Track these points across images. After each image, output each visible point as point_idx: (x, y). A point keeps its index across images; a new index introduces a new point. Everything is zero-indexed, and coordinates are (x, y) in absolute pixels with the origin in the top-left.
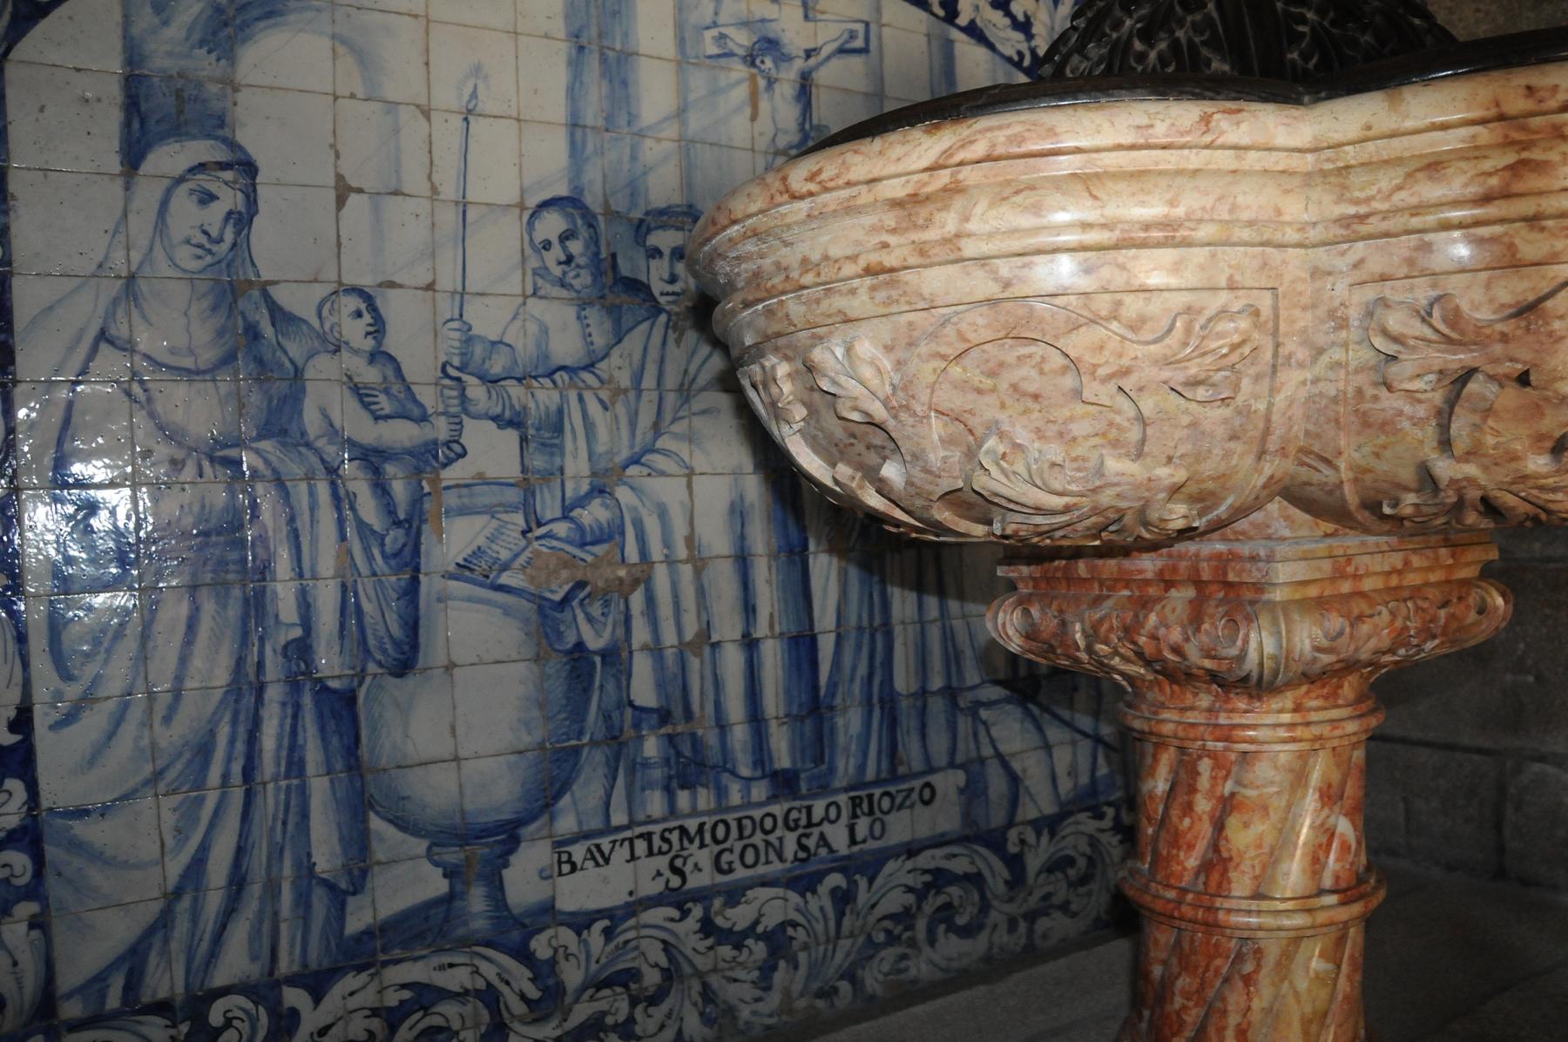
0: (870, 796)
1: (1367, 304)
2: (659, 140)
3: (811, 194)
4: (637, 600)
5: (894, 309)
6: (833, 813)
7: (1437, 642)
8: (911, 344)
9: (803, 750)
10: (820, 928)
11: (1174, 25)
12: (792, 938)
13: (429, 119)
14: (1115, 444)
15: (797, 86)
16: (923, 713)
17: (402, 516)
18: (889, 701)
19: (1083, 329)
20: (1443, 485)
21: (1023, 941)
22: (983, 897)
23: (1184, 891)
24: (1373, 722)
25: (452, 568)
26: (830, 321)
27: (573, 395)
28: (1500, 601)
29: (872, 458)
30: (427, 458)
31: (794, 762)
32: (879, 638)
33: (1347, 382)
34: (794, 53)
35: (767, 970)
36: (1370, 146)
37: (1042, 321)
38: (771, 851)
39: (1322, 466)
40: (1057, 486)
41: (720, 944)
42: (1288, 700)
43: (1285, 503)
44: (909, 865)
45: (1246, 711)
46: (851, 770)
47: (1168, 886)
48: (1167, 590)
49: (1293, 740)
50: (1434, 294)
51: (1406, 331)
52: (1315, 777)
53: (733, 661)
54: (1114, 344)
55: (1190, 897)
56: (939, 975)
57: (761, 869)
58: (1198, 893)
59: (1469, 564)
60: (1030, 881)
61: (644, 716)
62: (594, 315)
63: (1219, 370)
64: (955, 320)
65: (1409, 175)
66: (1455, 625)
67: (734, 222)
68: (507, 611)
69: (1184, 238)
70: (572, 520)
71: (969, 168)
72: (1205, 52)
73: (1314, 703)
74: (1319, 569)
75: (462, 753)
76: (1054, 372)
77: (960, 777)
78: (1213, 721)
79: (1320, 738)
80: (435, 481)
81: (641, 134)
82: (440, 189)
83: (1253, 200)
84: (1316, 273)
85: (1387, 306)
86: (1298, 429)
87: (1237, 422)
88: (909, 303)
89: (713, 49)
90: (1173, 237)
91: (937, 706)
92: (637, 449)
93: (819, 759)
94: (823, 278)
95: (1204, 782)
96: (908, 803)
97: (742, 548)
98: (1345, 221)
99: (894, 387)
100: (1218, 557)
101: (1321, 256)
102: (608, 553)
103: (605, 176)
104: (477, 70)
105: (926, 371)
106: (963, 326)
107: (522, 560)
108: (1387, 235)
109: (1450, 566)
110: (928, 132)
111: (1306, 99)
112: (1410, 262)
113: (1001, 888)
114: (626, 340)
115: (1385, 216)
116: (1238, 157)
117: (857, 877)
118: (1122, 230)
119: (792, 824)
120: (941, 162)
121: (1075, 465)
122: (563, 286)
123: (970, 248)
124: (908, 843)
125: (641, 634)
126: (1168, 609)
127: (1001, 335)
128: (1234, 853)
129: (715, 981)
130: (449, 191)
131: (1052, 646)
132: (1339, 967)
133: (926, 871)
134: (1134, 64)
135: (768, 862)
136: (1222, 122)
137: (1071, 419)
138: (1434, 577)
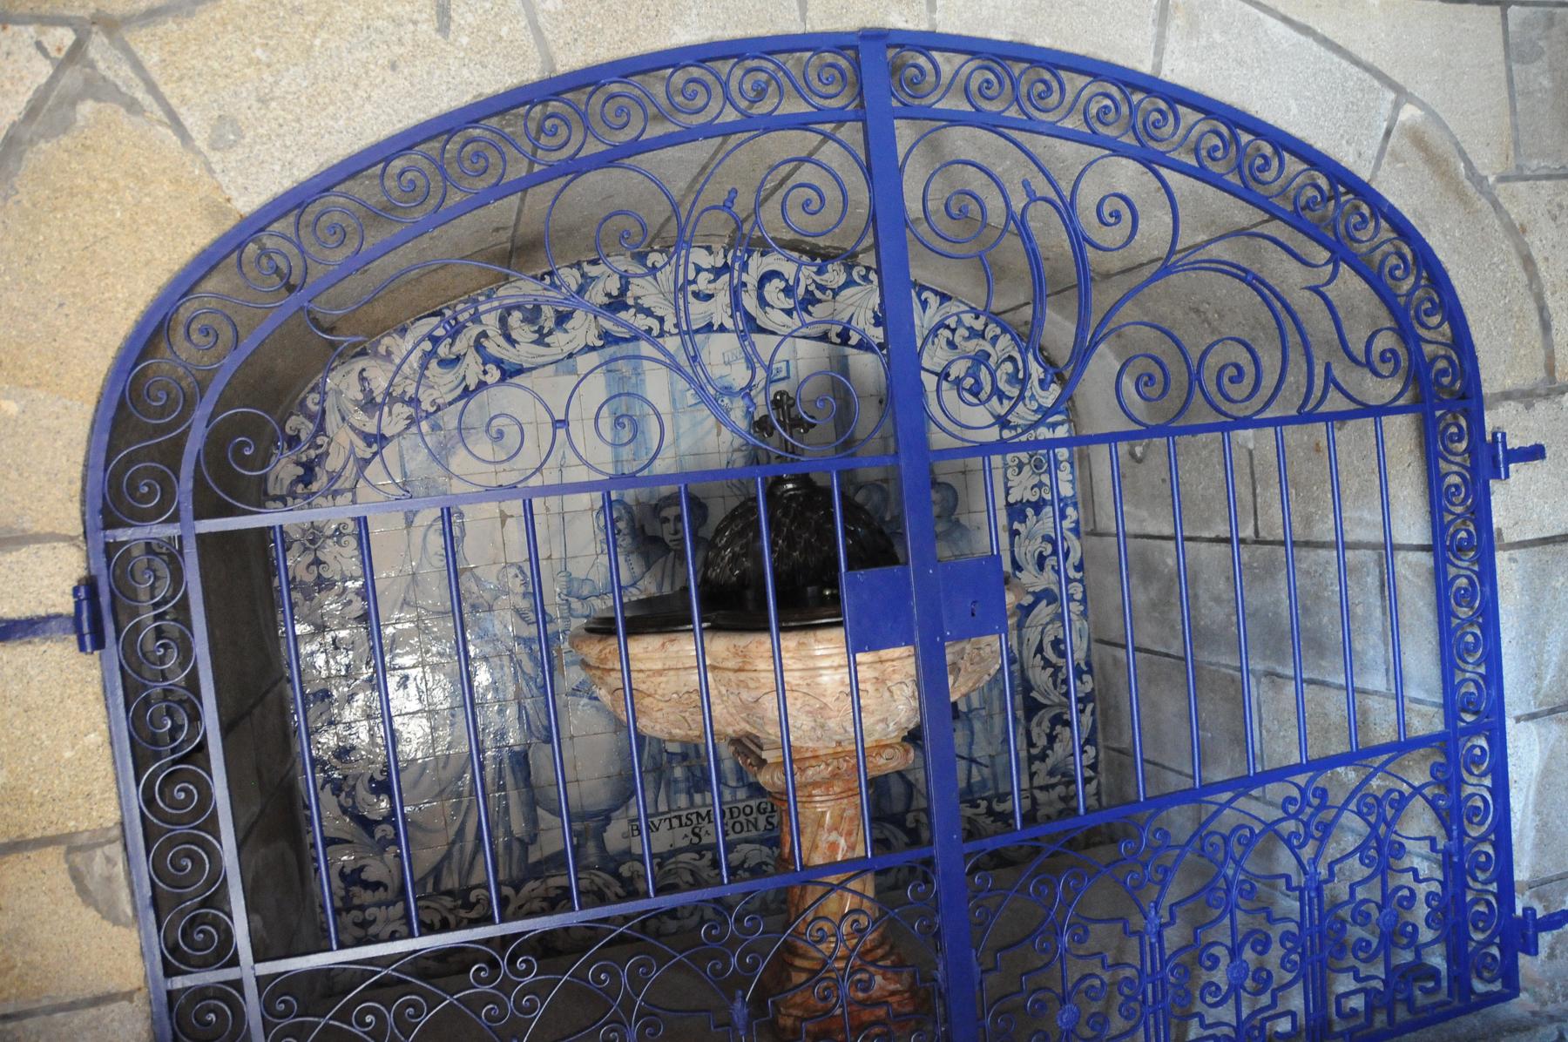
57: (744, 835)
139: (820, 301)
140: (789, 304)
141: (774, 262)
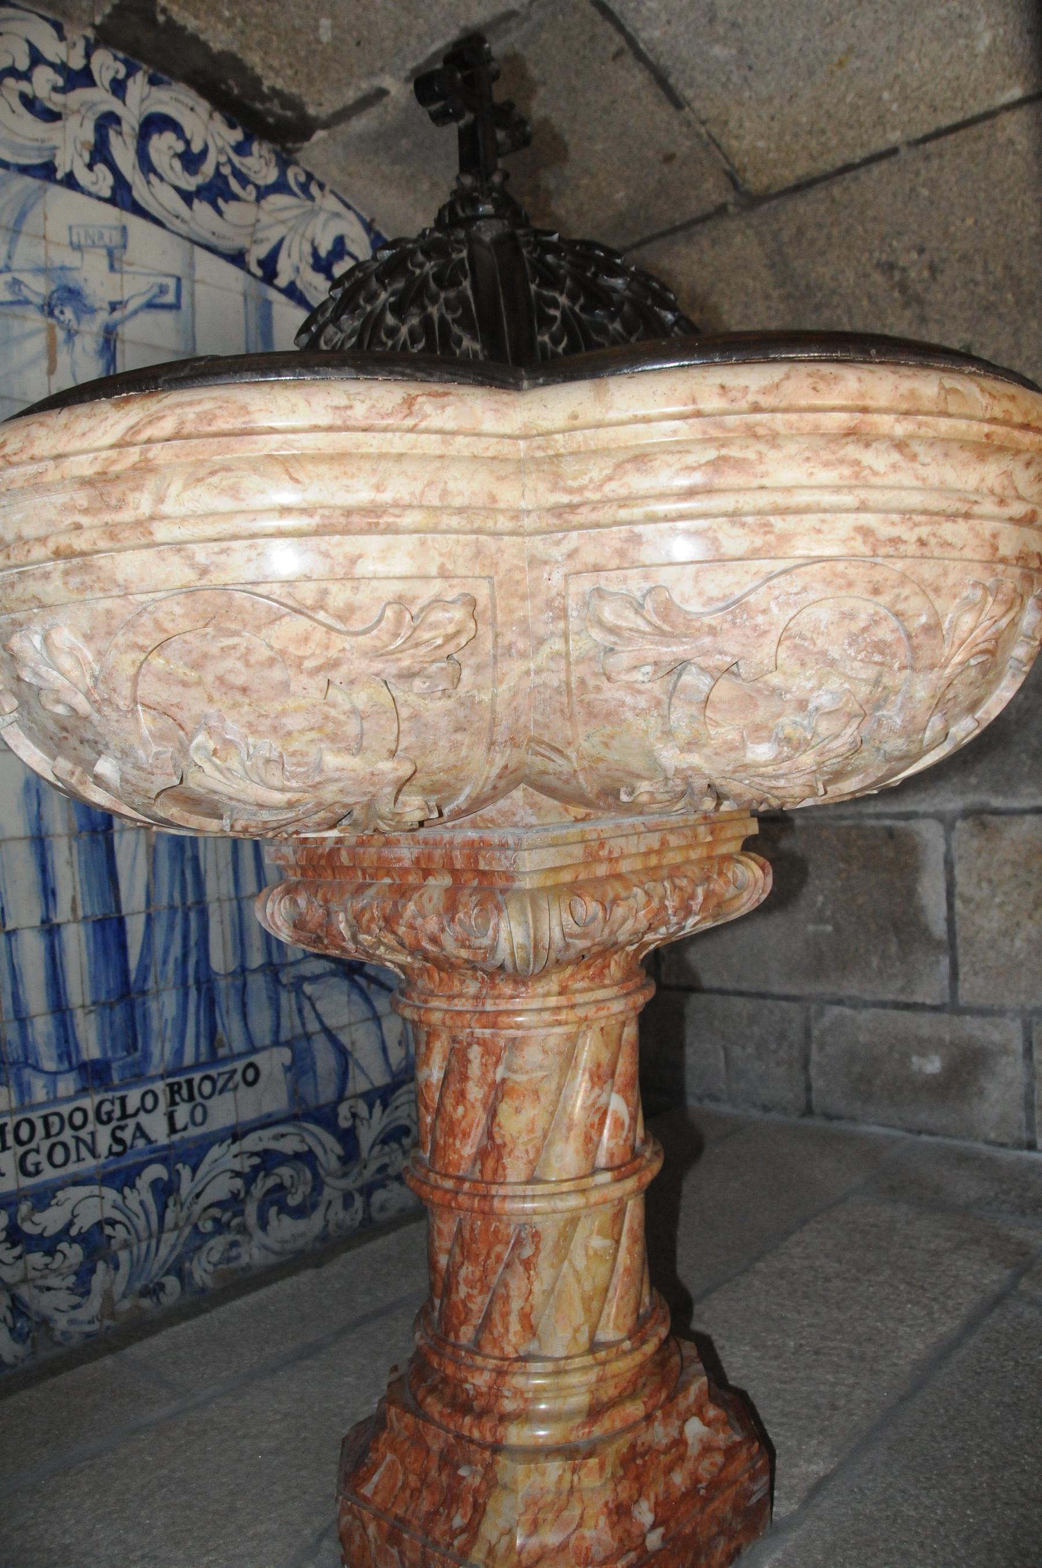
0: (190, 1082)
5: (88, 595)
6: (149, 1102)
9: (113, 1039)
10: (141, 1224)
12: (110, 1237)
14: (333, 738)
15: (101, 340)
18: (206, 982)
19: (287, 619)
21: (360, 1216)
22: (316, 1175)
23: (461, 1180)
24: (641, 999)
28: (759, 873)
29: (87, 752)
31: (104, 1051)
32: (193, 916)
33: (568, 671)
34: (97, 305)
35: (84, 1274)
36: (579, 435)
37: (241, 610)
38: (82, 1146)
39: (554, 756)
40: (276, 781)
41: (29, 1251)
44: (235, 1148)
45: (512, 997)
47: (446, 1176)
48: (425, 878)
49: (559, 1023)
50: (647, 586)
53: (32, 950)
55: (466, 1186)
56: (273, 1259)
57: (72, 1168)
58: (475, 1182)
59: (729, 840)
60: (364, 1154)
63: (433, 661)
64: (151, 608)
65: (618, 466)
69: (389, 525)
71: (159, 446)
72: (456, 329)
73: (580, 985)
74: (570, 855)
76: (261, 664)
77: (285, 1055)
87: (461, 713)
90: (377, 524)
91: (258, 984)
93: (132, 1046)
94: (13, 561)
95: (475, 1069)
96: (231, 1085)
97: (39, 829)
98: (558, 511)
99: (96, 678)
100: (471, 844)
101: (537, 545)
106: (160, 615)
108: (597, 525)
110: (117, 405)
111: (525, 384)
112: (621, 553)
113: (333, 1164)
115: (596, 505)
117: (179, 1166)
118: (323, 516)
119: (105, 1118)
120: (128, 438)
121: (294, 760)
123: (162, 532)
124: (234, 1127)
128: (508, 1139)
129: (25, 1292)
132: (618, 1242)
133: (253, 1154)
134: (384, 338)
135: (79, 1159)
136: (426, 405)
137: (284, 713)
138: (694, 855)
139: (236, 198)
140: (190, 183)
141: (176, 101)
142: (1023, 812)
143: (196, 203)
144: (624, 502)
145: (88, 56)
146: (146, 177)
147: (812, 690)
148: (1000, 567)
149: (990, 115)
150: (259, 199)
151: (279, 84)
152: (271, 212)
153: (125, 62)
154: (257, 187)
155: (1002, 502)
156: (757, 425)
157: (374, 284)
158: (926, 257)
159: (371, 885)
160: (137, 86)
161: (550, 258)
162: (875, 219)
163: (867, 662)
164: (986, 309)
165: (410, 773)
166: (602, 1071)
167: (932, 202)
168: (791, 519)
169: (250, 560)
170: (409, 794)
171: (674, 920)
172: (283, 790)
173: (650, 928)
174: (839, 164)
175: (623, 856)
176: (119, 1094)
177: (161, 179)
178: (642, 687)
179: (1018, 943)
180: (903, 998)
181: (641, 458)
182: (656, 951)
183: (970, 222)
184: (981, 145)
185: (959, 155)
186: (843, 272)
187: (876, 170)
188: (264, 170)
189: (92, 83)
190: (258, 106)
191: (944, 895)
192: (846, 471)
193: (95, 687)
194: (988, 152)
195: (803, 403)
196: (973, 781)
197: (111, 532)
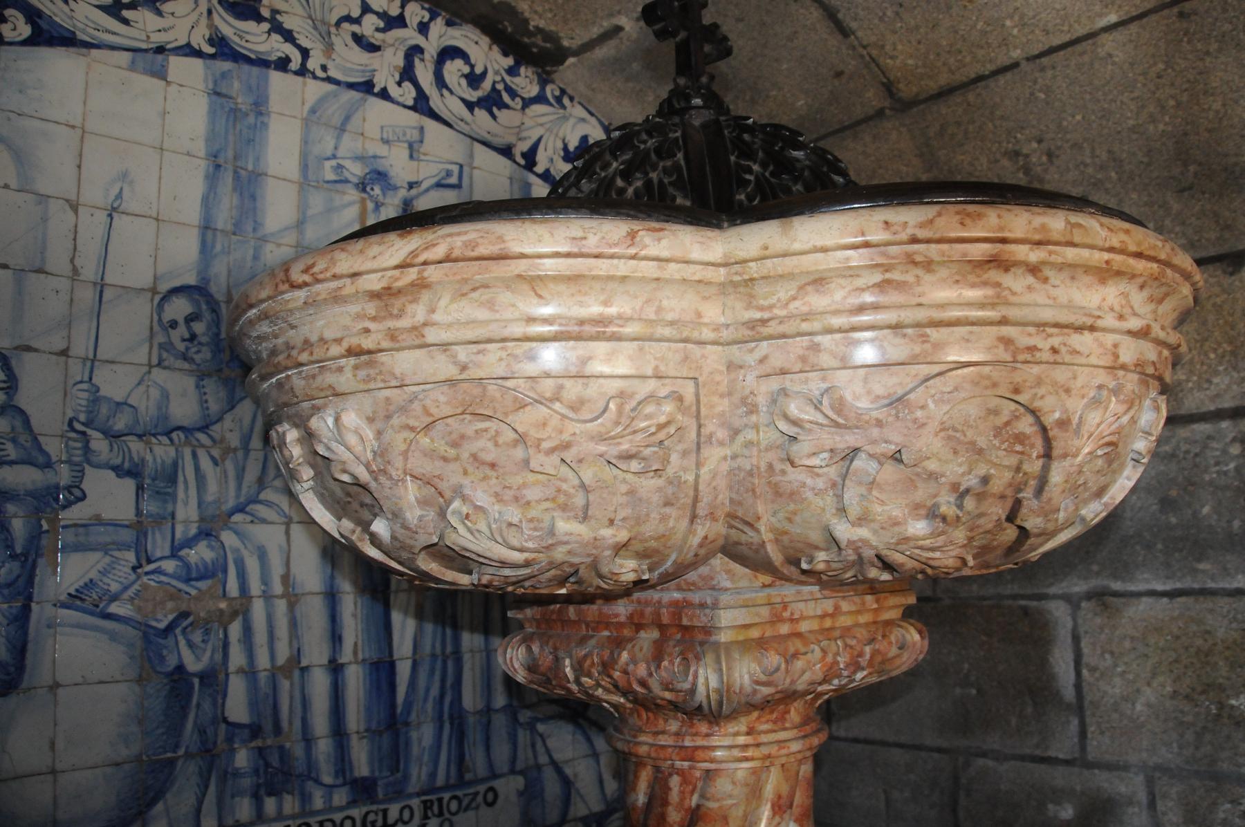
0: (440, 800)
1: (772, 393)
2: (279, 245)
3: (306, 284)
4: (235, 629)
5: (372, 385)
7: (865, 673)
8: (388, 417)
11: (648, 168)
13: (76, 211)
14: (564, 508)
16: (487, 726)
17: (19, 550)
18: (458, 718)
19: (529, 407)
20: (843, 545)
24: (815, 741)
25: (63, 597)
26: (323, 394)
27: (187, 452)
28: (917, 637)
29: (366, 515)
30: (46, 501)
31: (373, 771)
32: (450, 664)
36: (768, 263)
39: (746, 529)
40: (515, 543)
42: (741, 725)
43: (726, 559)
45: (708, 735)
46: (424, 777)
48: (637, 631)
49: (747, 759)
50: (824, 386)
51: (803, 416)
52: (769, 790)
53: (320, 683)
54: (555, 421)
61: (237, 731)
62: (211, 385)
65: (801, 288)
66: (879, 659)
67: (251, 306)
68: (113, 637)
69: (614, 333)
70: (180, 559)
71: (433, 267)
72: (671, 190)
74: (758, 615)
75: (59, 766)
76: (507, 444)
77: (519, 782)
78: (680, 744)
79: (769, 756)
80: (54, 521)
81: (264, 239)
82: (80, 271)
83: (676, 304)
84: (732, 366)
85: (786, 395)
86: (724, 497)
87: (670, 490)
88: (384, 381)
89: (330, 176)
91: (500, 722)
92: (242, 499)
93: (395, 769)
94: (315, 357)
95: (674, 796)
96: (474, 805)
97: (332, 586)
98: (752, 325)
99: (375, 453)
100: (675, 604)
102: (210, 588)
103: (229, 271)
104: (124, 176)
105: (398, 440)
106: (428, 402)
107: (130, 592)
108: (784, 336)
109: (876, 610)
110: (401, 236)
111: (726, 225)
112: (803, 359)
114: (239, 407)
116: (659, 267)
121: (532, 525)
122: (185, 359)
123: (432, 336)
125: (237, 658)
126: (637, 648)
127: (459, 411)
130: (89, 271)
131: (548, 679)
137: (524, 485)
138: (863, 619)
139: (507, 107)
140: (473, 96)
142: (1139, 595)
143: (476, 110)
144: (806, 318)
145: (403, 7)
146: (440, 90)
147: (963, 474)
148: (1121, 373)
149: (1092, 35)
150: (523, 108)
151: (542, 24)
152: (531, 118)
153: (429, 10)
154: (523, 99)
155: (1121, 317)
156: (915, 253)
157: (608, 157)
158: (1044, 145)
159: (592, 637)
160: (437, 27)
161: (746, 137)
162: (1002, 118)
163: (1010, 451)
164: (1095, 184)
165: (626, 539)
166: (782, 801)
167: (1047, 103)
168: (945, 331)
169: (501, 359)
170: (625, 558)
171: (845, 673)
172: (521, 550)
173: (825, 680)
174: (973, 76)
175: (803, 618)
176: (382, 807)
177: (451, 92)
178: (820, 471)
179: (1139, 707)
180: (1038, 752)
181: (819, 281)
182: (828, 702)
183: (1079, 117)
184: (1086, 58)
185: (1067, 66)
186: (977, 159)
187: (1002, 80)
188: (529, 87)
189: (405, 26)
190: (526, 40)
191: (1072, 664)
192: (989, 292)
193: (374, 459)
194: (1092, 64)
195: (953, 235)
196: (1095, 568)
197: (392, 335)
